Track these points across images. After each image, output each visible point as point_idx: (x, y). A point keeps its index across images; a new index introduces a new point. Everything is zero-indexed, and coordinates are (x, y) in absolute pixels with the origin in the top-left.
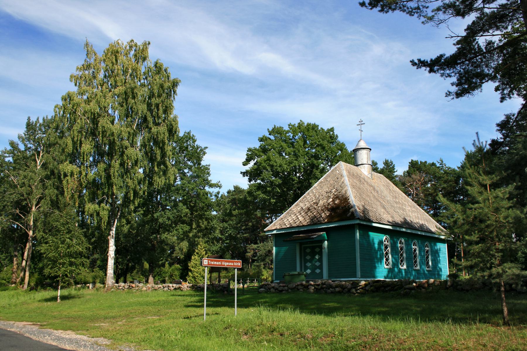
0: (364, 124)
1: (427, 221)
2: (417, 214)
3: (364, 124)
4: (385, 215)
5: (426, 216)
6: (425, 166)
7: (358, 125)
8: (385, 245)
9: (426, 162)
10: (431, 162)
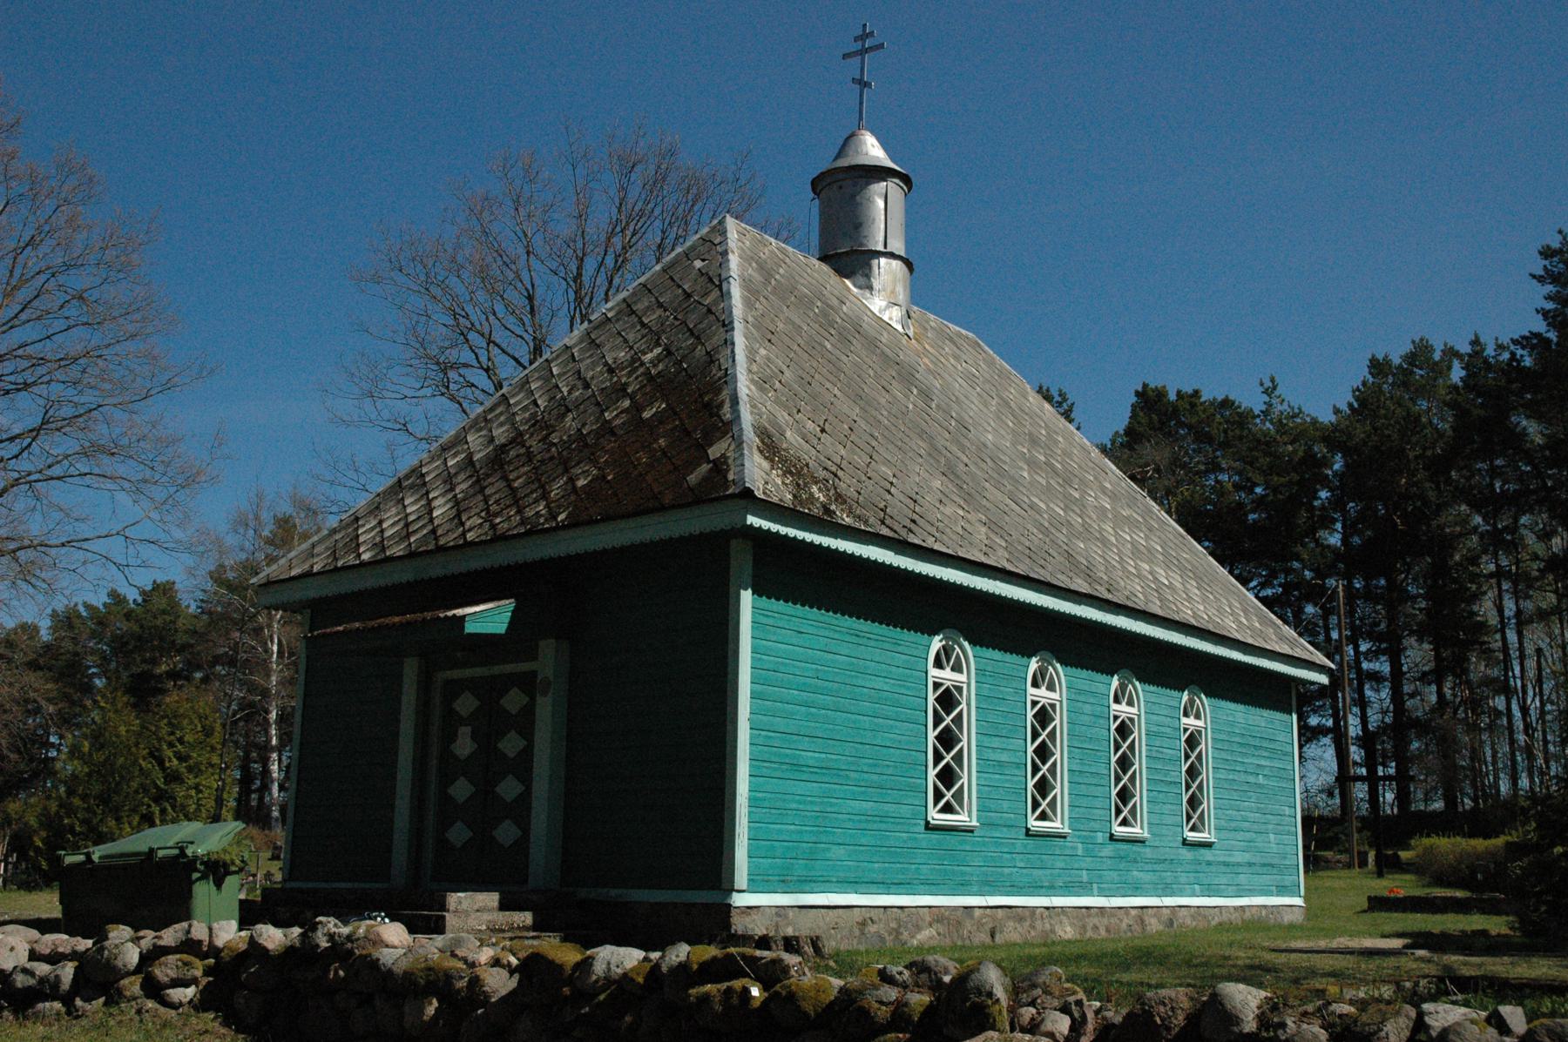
0: (881, 46)
1: (1198, 578)
2: (1147, 538)
3: (881, 46)
4: (948, 510)
5: (1192, 551)
6: (1193, 405)
7: (845, 56)
8: (937, 685)
9: (1196, 393)
10: (1220, 398)
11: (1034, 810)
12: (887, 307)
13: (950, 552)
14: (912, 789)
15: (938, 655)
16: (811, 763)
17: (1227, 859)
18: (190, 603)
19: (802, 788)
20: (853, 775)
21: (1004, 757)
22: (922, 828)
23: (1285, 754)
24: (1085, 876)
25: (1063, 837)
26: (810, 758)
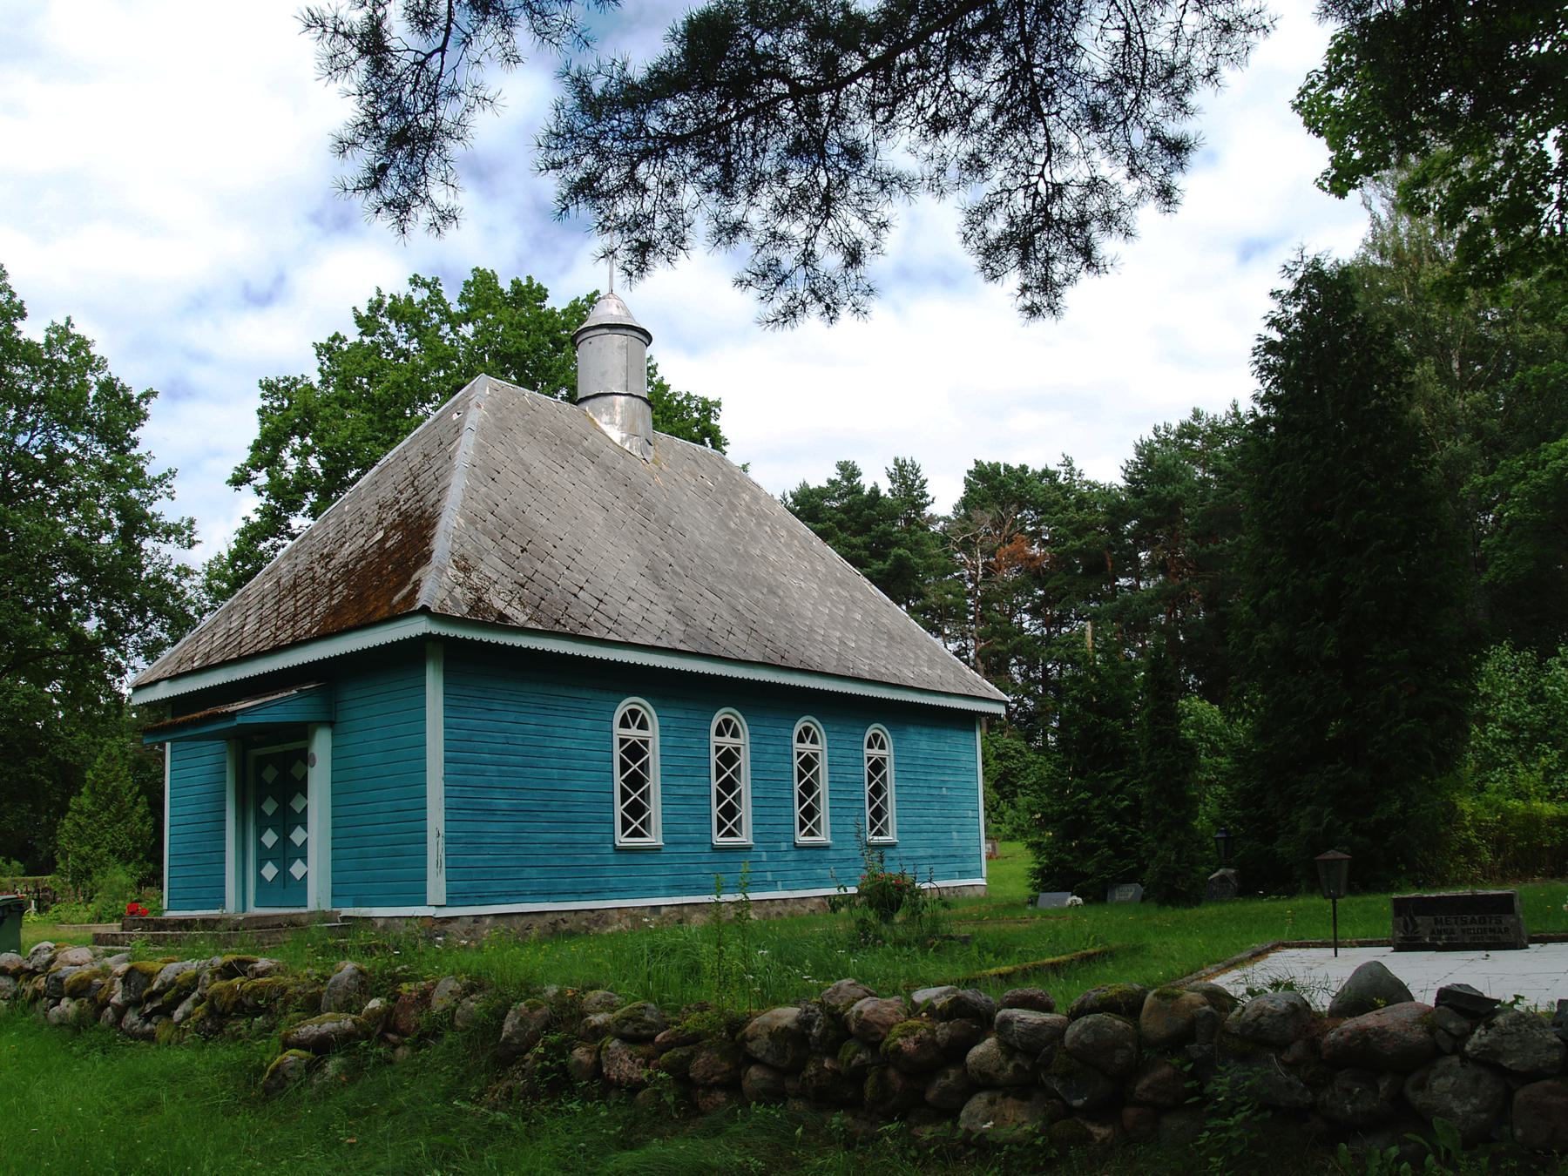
11: (801, 830)
12: (628, 438)
13: (622, 639)
14: (602, 821)
15: (624, 718)
16: (505, 807)
17: (911, 854)
18: (548, 304)
19: (494, 827)
20: (543, 814)
21: (689, 791)
22: (611, 851)
23: (971, 770)
24: (769, 877)
25: (749, 848)
26: (503, 804)
